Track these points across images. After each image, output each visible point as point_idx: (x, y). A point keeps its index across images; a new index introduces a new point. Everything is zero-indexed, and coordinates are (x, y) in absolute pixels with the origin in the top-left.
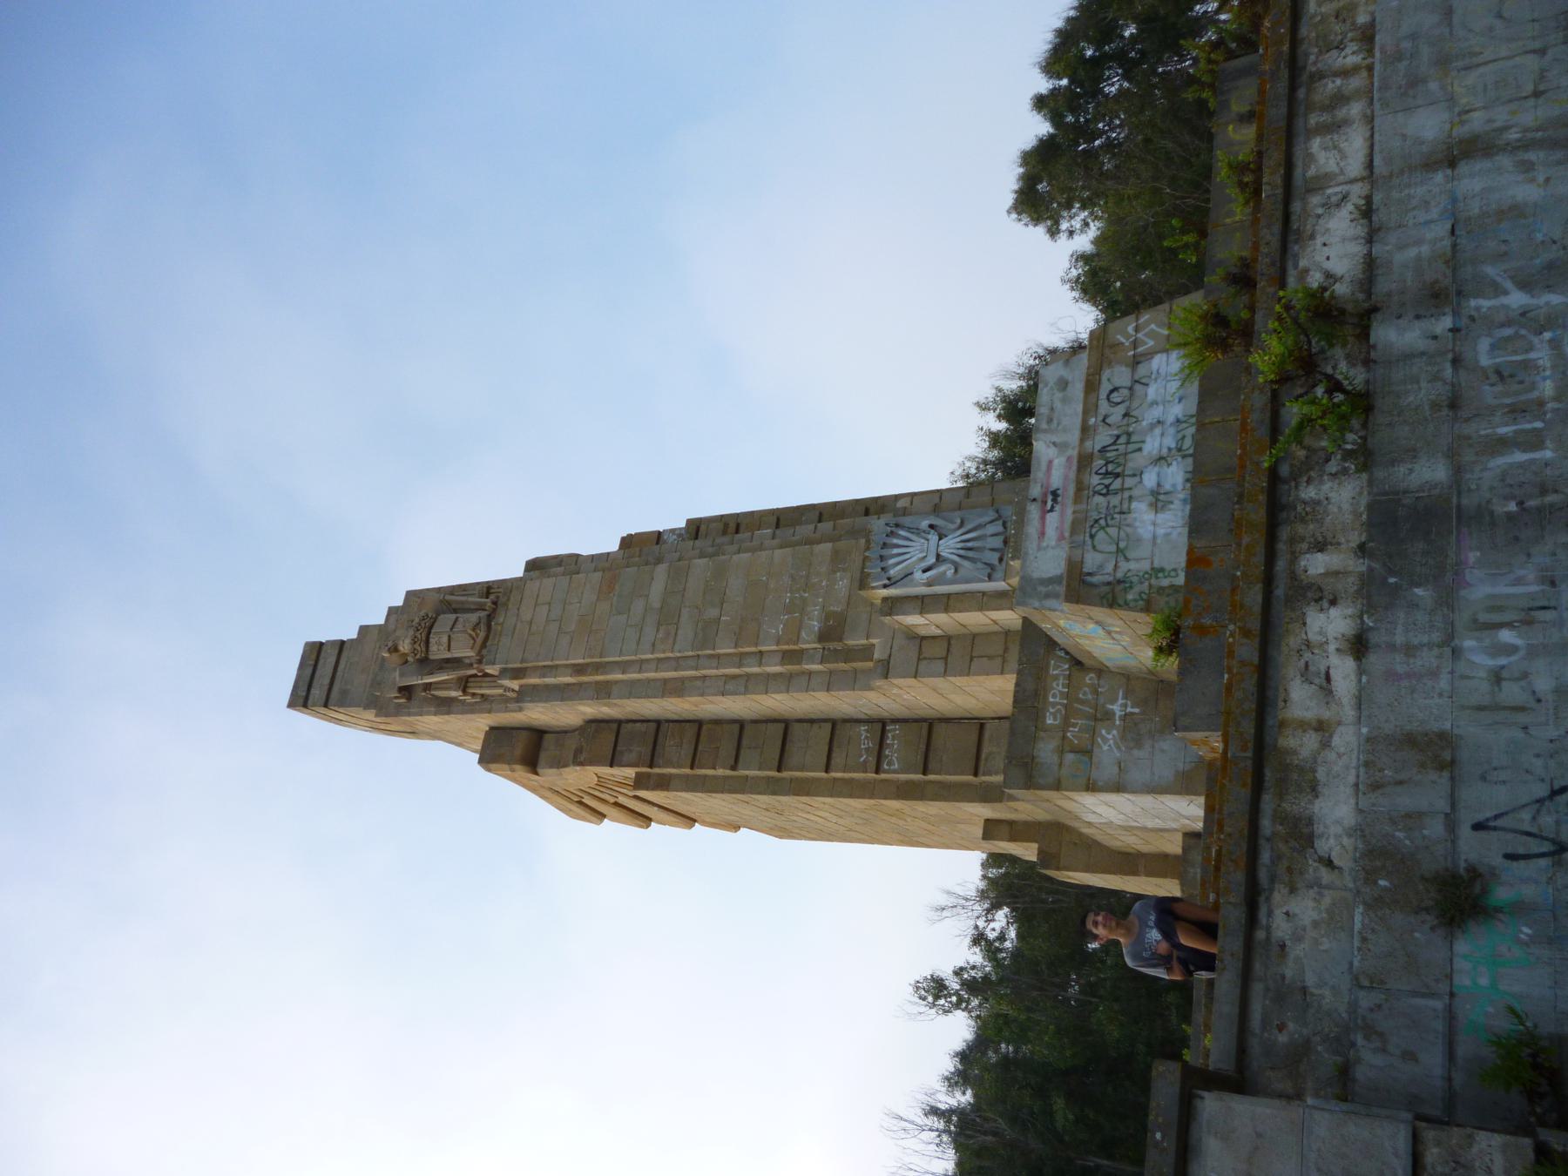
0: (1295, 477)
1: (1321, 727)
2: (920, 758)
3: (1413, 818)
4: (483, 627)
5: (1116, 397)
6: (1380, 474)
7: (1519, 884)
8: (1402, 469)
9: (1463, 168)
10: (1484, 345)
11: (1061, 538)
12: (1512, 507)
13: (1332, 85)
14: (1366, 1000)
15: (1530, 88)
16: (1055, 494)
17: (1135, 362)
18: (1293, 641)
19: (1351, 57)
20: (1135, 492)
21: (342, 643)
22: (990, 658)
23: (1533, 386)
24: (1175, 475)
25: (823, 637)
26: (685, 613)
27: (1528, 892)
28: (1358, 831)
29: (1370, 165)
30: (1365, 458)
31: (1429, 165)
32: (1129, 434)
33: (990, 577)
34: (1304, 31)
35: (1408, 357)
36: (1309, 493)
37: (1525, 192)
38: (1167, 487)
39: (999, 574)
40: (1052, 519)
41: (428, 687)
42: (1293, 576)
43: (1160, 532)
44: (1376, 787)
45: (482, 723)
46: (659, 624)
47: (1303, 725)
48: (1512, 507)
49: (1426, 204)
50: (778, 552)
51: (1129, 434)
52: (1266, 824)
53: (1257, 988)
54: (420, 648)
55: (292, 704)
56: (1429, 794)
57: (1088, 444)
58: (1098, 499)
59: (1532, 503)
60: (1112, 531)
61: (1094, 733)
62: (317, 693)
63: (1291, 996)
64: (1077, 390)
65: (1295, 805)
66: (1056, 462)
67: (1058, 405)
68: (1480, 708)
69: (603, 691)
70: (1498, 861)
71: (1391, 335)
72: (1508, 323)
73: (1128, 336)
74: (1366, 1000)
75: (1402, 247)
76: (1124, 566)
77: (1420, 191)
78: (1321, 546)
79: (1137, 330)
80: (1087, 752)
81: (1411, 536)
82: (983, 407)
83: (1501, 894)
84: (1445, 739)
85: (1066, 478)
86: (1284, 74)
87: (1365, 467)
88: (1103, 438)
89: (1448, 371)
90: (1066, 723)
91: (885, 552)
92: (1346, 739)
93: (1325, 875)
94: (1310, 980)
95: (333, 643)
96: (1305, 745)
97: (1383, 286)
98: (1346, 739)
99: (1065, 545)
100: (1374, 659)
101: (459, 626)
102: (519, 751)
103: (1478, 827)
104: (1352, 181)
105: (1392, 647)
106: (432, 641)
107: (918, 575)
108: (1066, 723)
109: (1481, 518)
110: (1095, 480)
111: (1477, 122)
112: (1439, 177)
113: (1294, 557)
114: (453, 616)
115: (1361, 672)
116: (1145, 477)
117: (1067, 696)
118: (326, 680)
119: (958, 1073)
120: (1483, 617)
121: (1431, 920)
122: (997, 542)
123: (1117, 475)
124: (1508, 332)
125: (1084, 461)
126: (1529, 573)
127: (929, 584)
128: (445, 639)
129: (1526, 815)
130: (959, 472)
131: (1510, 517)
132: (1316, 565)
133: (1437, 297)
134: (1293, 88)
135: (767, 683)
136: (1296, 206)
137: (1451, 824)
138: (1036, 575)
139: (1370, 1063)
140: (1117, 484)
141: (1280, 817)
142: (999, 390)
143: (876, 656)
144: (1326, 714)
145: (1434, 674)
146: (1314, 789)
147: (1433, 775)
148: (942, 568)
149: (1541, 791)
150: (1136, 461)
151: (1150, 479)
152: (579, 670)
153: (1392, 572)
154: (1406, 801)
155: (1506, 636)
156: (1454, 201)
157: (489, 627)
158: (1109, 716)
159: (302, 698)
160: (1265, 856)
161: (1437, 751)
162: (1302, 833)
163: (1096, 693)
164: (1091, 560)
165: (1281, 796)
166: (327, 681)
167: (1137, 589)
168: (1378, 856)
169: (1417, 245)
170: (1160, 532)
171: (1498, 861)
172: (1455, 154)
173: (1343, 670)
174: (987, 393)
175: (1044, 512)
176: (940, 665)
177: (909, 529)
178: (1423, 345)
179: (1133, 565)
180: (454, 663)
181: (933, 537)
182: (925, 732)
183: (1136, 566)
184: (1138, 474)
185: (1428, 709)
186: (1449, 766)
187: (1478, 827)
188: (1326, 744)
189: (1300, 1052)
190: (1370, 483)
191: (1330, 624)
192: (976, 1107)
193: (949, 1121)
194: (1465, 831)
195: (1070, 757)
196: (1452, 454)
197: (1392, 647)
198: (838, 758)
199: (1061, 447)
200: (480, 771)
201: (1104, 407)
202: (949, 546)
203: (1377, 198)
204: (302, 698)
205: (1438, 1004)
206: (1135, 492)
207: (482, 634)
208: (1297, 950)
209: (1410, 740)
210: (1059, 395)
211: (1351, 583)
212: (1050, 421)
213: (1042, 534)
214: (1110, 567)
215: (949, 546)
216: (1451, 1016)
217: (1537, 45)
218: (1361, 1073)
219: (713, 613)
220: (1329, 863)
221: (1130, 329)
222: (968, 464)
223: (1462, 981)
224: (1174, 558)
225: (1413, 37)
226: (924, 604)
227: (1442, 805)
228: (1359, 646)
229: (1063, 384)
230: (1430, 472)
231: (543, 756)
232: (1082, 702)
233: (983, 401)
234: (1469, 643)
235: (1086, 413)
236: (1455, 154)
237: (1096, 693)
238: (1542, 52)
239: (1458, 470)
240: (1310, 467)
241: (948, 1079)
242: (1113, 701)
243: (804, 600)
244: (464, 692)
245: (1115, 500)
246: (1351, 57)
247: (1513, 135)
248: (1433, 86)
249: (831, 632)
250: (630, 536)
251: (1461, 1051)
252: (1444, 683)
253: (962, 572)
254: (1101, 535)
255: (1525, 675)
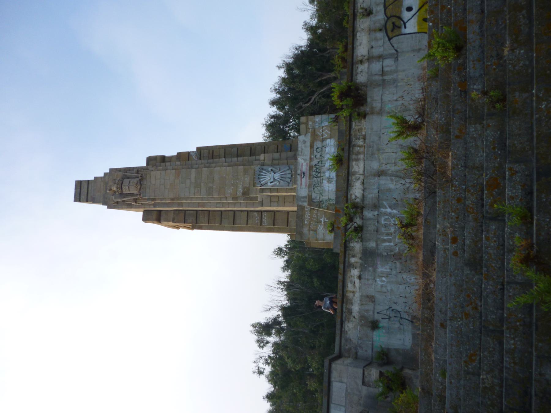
0: (349, 241)
1: (353, 292)
2: (272, 222)
3: (367, 311)
4: (139, 184)
5: (318, 150)
6: (364, 244)
7: (383, 323)
8: (368, 243)
9: (381, 177)
10: (383, 219)
11: (306, 186)
12: (386, 254)
13: (357, 149)
14: (360, 342)
15: (393, 161)
16: (304, 173)
17: (323, 141)
18: (349, 275)
19: (361, 142)
20: (324, 178)
21: (88, 181)
22: (290, 202)
23: (390, 230)
24: (333, 174)
25: (244, 194)
26: (202, 184)
27: (385, 325)
28: (359, 312)
29: (364, 171)
30: (362, 240)
31: (375, 175)
32: (322, 161)
33: (288, 186)
34: (352, 132)
35: (370, 219)
36: (352, 245)
37: (392, 186)
38: (331, 177)
39: (291, 185)
40: (304, 180)
41: (123, 201)
42: (349, 262)
43: (330, 189)
44: (362, 305)
45: (143, 209)
46: (195, 188)
47: (350, 292)
48: (386, 254)
49: (374, 185)
50: (228, 168)
51: (322, 161)
52: (344, 309)
53: (343, 339)
54: (120, 190)
55: (76, 200)
56: (370, 307)
57: (312, 163)
58: (315, 179)
59: (389, 254)
60: (319, 188)
61: (317, 226)
62: (83, 197)
63: (348, 340)
64: (308, 144)
65: (349, 306)
66: (304, 164)
67: (303, 148)
68: (379, 292)
69: (181, 205)
70: (380, 319)
71: (368, 214)
72: (387, 215)
73: (320, 133)
74: (360, 342)
75: (369, 194)
76: (322, 197)
77: (373, 181)
78: (354, 256)
79: (323, 131)
80: (315, 231)
81: (369, 256)
82: (279, 67)
83: (381, 325)
84: (373, 297)
85: (306, 169)
86: (348, 145)
87: (362, 241)
88: (315, 162)
89: (376, 224)
90: (310, 223)
91: (260, 177)
92: (357, 295)
93: (354, 320)
94: (351, 338)
95: (85, 181)
96: (350, 295)
97: (366, 202)
98: (357, 295)
99: (307, 187)
100: (362, 280)
101: (131, 184)
102: (153, 216)
103: (378, 313)
104: (361, 175)
105: (365, 279)
106: (123, 188)
107: (269, 184)
108: (310, 223)
109: (380, 255)
110: (314, 173)
111: (384, 167)
112: (376, 179)
113: (349, 258)
114: (128, 180)
115: (360, 283)
116: (326, 174)
117: (310, 216)
118: (85, 192)
119: (286, 266)
120: (380, 275)
121: (370, 329)
122: (289, 176)
123: (319, 173)
124: (387, 217)
125: (311, 168)
126: (388, 267)
127: (272, 186)
128: (127, 188)
129: (385, 311)
130: (273, 88)
131: (385, 256)
132: (353, 260)
133: (376, 207)
134: (349, 147)
135: (229, 204)
136: (350, 178)
137: (374, 312)
138: (300, 195)
139: (361, 352)
140: (319, 175)
141: (346, 309)
142: (284, 61)
143: (259, 200)
144: (354, 290)
145: (372, 285)
146: (352, 304)
147: (371, 303)
148: (275, 183)
149: (388, 307)
150: (324, 169)
151: (327, 174)
152: (173, 199)
153: (366, 264)
154: (366, 307)
155: (384, 279)
156: (379, 185)
157: (141, 185)
158: (321, 222)
159: (78, 198)
160: (344, 315)
161: (372, 299)
162: (350, 312)
163: (317, 215)
164: (314, 195)
165: (347, 304)
166: (86, 193)
167: (325, 204)
168: (362, 317)
169: (372, 195)
170: (330, 189)
171: (380, 319)
172: (380, 174)
173: (357, 281)
174: (280, 62)
175: (302, 178)
176: (276, 204)
177: (266, 170)
178: (372, 217)
179: (324, 197)
180: (132, 194)
181: (272, 173)
182: (273, 214)
183: (325, 198)
184: (324, 173)
185: (371, 291)
186: (373, 302)
187: (378, 313)
188: (354, 296)
189: (350, 349)
190: (362, 245)
191: (355, 272)
192: (292, 272)
193: (284, 286)
194: (376, 314)
195: (311, 232)
196: (376, 242)
197: (365, 279)
198: (250, 222)
199: (305, 160)
200: (143, 222)
201: (315, 153)
202: (277, 176)
203: (365, 181)
204: (78, 198)
205: (371, 343)
206: (324, 178)
207: (139, 187)
208: (349, 332)
209: (367, 297)
210: (303, 145)
211: (358, 265)
212: (302, 152)
213: (301, 184)
214: (318, 198)
215: (277, 176)
216: (373, 345)
217: (395, 151)
218: (359, 354)
219: (211, 185)
220: (354, 317)
221: (321, 131)
222: (276, 85)
223: (375, 339)
224: (333, 196)
225: (373, 142)
226: (271, 190)
227: (372, 309)
228: (360, 277)
229: (304, 142)
230: (372, 245)
231: (162, 218)
232: (314, 218)
233: (279, 65)
234: (378, 279)
235: (311, 154)
236: (380, 174)
237: (317, 215)
238: (396, 153)
239: (377, 245)
240: (351, 240)
241: (283, 268)
242: (322, 218)
243: (237, 183)
244: (136, 203)
245: (319, 179)
246: (361, 142)
247: (390, 172)
248: (376, 156)
249: (246, 193)
250: (180, 153)
251: (374, 350)
252: (373, 287)
253: (281, 184)
254: (316, 189)
255: (386, 287)
